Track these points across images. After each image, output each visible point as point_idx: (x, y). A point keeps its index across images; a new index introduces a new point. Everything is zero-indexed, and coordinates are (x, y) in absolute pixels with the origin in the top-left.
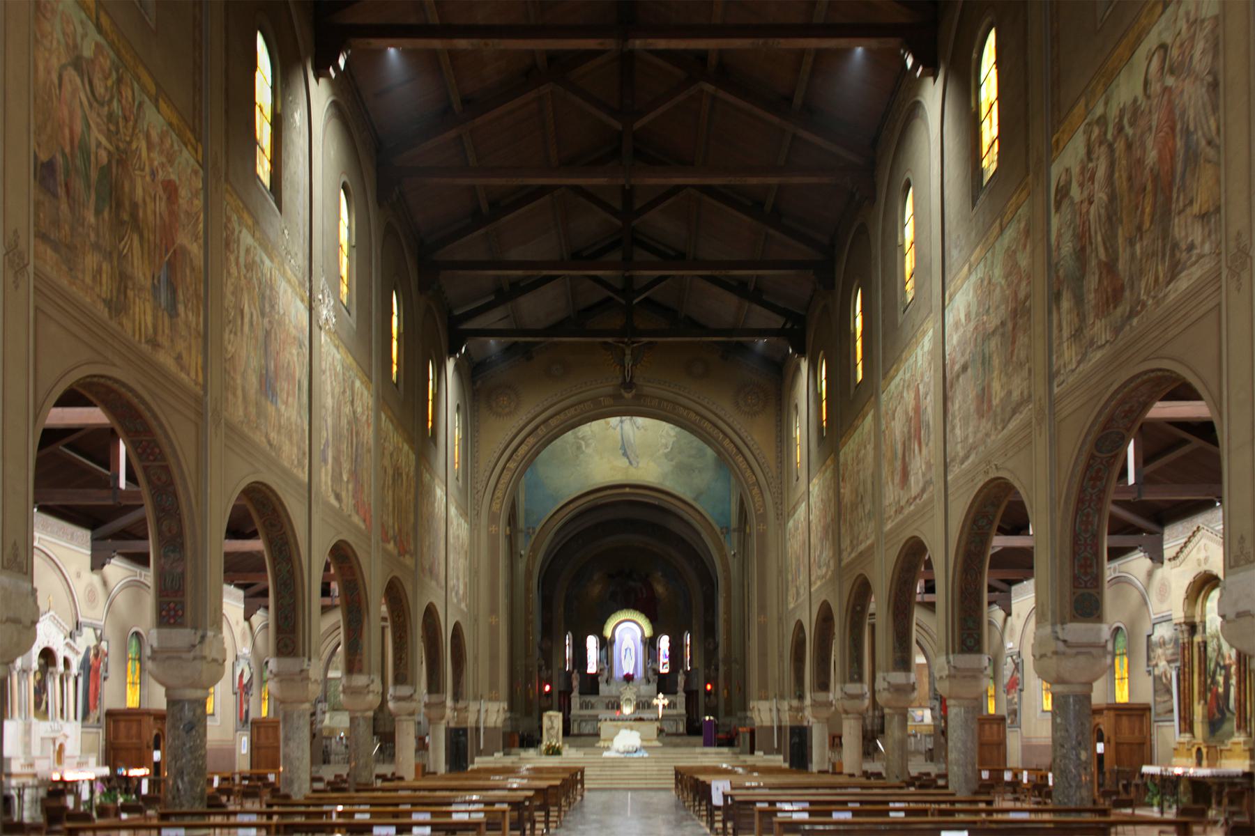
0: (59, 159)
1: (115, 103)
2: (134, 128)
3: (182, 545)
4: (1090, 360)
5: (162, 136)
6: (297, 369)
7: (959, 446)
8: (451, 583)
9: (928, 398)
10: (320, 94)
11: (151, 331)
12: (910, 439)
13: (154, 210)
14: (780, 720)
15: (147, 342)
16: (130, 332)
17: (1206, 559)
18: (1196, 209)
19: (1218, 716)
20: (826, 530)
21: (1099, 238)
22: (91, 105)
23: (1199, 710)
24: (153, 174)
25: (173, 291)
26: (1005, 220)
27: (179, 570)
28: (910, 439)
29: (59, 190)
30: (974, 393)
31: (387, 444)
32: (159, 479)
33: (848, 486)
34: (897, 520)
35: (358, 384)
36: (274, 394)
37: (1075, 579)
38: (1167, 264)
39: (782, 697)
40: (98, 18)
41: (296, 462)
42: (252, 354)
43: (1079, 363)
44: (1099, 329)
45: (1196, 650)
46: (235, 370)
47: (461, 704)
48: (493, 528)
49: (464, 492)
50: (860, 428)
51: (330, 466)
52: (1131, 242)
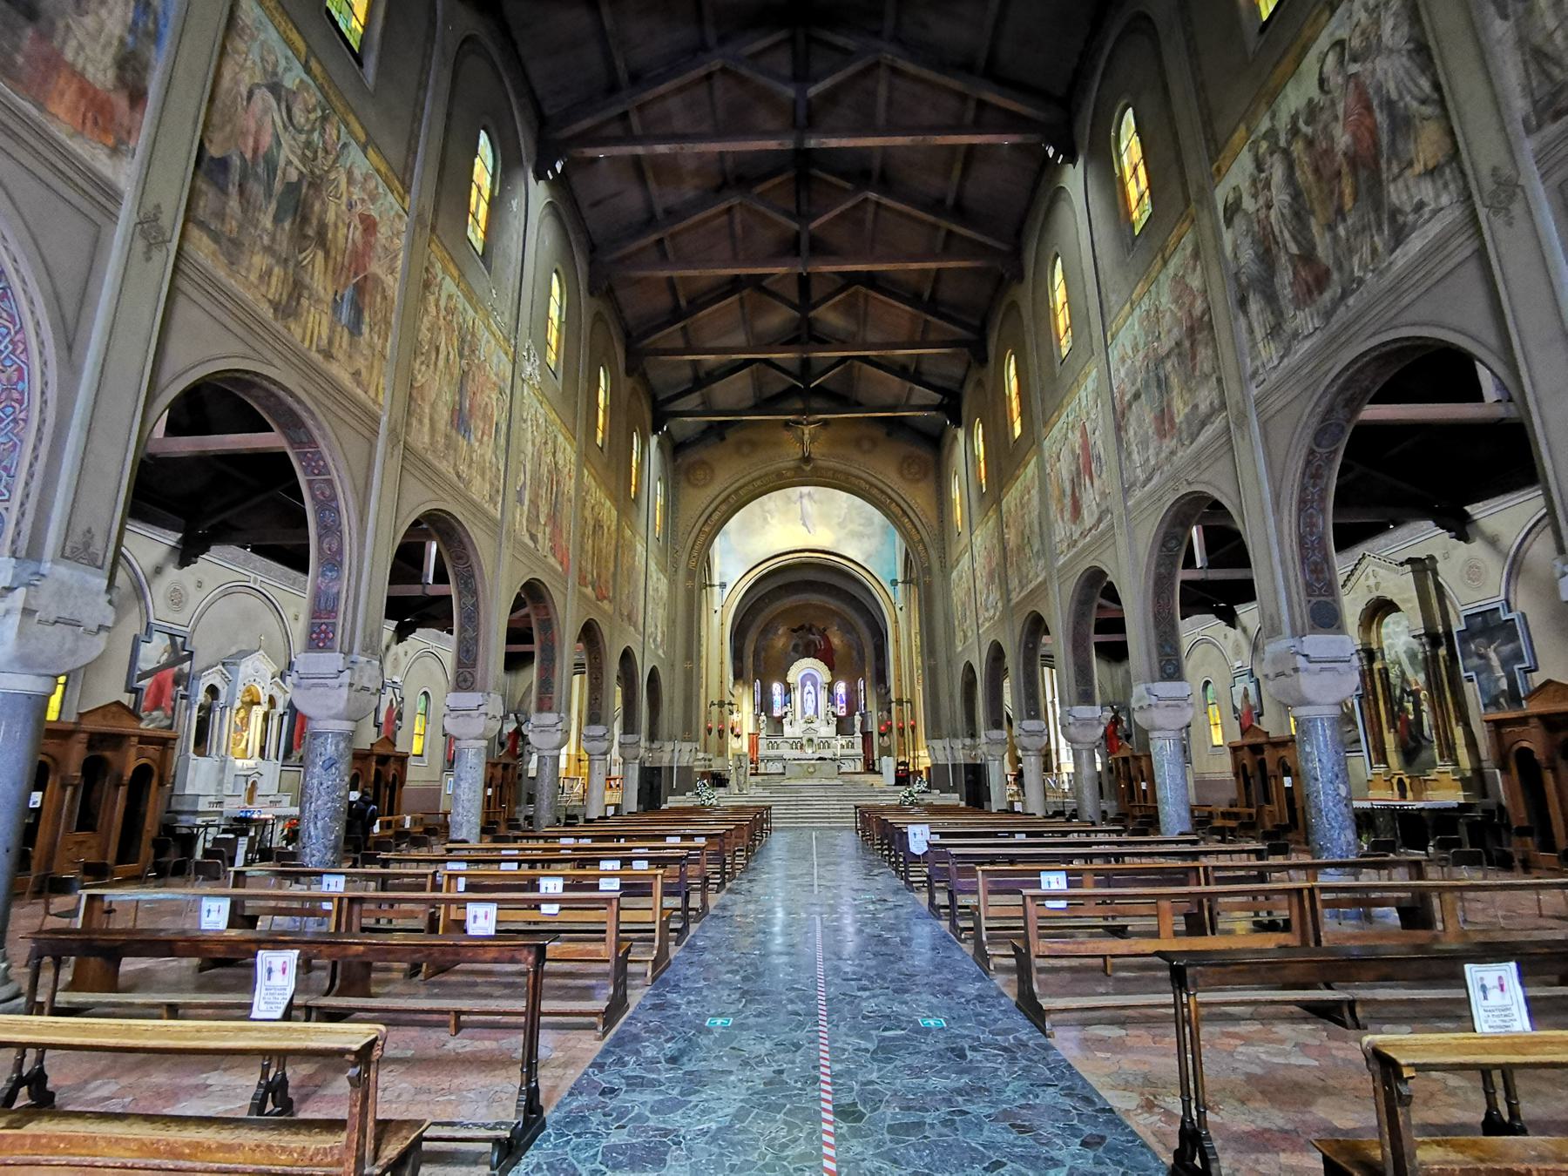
0: (236, 161)
1: (316, 135)
2: (335, 161)
3: (341, 563)
4: (1296, 353)
5: (366, 178)
6: (495, 414)
7: (1138, 470)
8: (650, 630)
9: (1097, 433)
10: (539, 193)
11: (325, 341)
12: (1079, 474)
13: (346, 236)
14: (954, 758)
15: (318, 351)
16: (298, 338)
17: (1377, 585)
18: (1419, 168)
19: (1412, 744)
20: (991, 575)
21: (1287, 235)
22: (285, 127)
23: (1390, 739)
24: (351, 206)
25: (358, 311)
26: (1167, 254)
27: (335, 590)
28: (1079, 474)
29: (230, 187)
30: (1152, 415)
31: (588, 497)
32: (323, 494)
33: (1013, 531)
34: (1071, 553)
35: (561, 438)
36: (467, 431)
37: (1309, 586)
38: (1386, 232)
39: (956, 736)
40: (307, 61)
41: (487, 498)
42: (445, 389)
43: (1282, 358)
44: (1303, 319)
45: (1377, 676)
46: (423, 399)
47: (656, 745)
48: (690, 584)
49: (664, 551)
50: (1022, 478)
51: (526, 508)
52: (1331, 227)
